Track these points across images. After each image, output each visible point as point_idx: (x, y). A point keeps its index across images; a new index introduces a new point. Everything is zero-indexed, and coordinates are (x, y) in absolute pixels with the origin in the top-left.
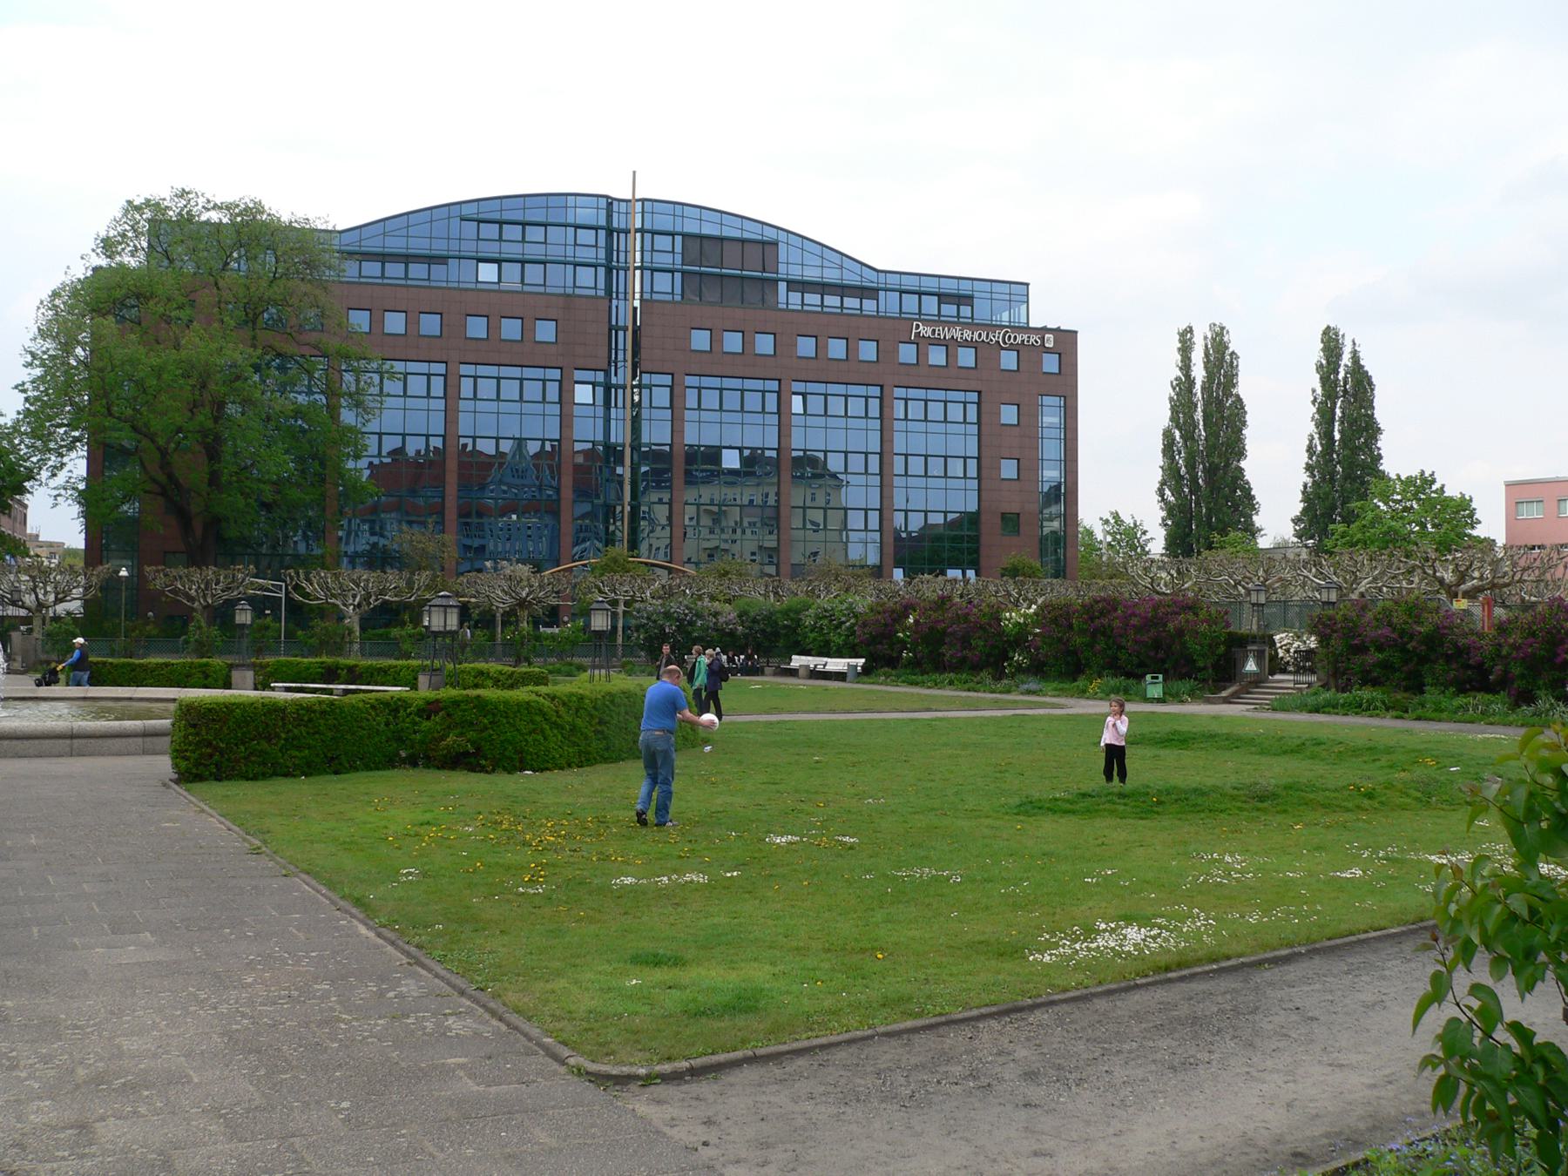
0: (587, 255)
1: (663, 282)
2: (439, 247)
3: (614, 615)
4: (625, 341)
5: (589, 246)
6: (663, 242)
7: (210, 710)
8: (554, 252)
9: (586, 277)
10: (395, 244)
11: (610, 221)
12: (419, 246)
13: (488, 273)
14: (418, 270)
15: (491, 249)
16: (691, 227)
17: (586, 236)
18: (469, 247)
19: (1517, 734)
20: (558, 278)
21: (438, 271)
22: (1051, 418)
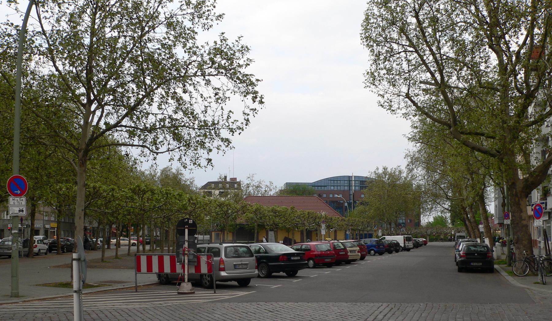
0: (346, 185)
1: (357, 188)
2: (326, 185)
3: (192, 245)
4: (352, 196)
5: (346, 183)
6: (357, 182)
7: (503, 205)
8: (342, 184)
9: (346, 188)
10: (319, 184)
11: (349, 179)
12: (323, 185)
13: (332, 188)
14: (323, 188)
15: (332, 184)
16: (361, 180)
17: (346, 182)
18: (330, 184)
19: (238, 221)
20: (342, 188)
21: (325, 188)
22: (282, 274)
